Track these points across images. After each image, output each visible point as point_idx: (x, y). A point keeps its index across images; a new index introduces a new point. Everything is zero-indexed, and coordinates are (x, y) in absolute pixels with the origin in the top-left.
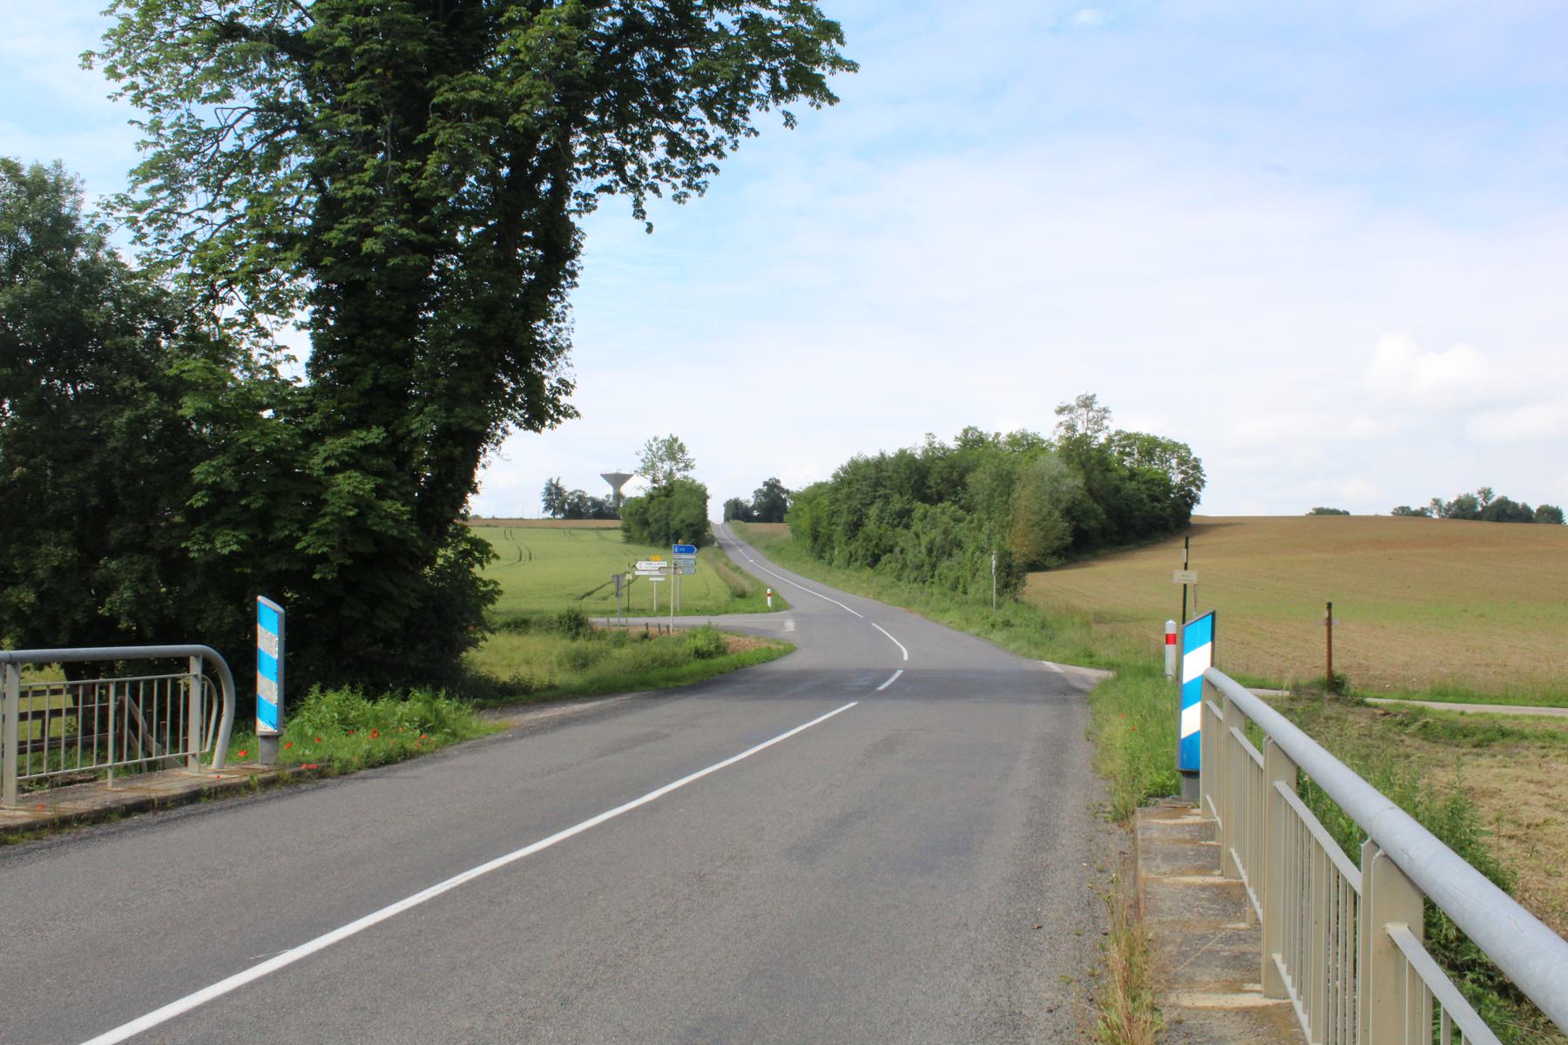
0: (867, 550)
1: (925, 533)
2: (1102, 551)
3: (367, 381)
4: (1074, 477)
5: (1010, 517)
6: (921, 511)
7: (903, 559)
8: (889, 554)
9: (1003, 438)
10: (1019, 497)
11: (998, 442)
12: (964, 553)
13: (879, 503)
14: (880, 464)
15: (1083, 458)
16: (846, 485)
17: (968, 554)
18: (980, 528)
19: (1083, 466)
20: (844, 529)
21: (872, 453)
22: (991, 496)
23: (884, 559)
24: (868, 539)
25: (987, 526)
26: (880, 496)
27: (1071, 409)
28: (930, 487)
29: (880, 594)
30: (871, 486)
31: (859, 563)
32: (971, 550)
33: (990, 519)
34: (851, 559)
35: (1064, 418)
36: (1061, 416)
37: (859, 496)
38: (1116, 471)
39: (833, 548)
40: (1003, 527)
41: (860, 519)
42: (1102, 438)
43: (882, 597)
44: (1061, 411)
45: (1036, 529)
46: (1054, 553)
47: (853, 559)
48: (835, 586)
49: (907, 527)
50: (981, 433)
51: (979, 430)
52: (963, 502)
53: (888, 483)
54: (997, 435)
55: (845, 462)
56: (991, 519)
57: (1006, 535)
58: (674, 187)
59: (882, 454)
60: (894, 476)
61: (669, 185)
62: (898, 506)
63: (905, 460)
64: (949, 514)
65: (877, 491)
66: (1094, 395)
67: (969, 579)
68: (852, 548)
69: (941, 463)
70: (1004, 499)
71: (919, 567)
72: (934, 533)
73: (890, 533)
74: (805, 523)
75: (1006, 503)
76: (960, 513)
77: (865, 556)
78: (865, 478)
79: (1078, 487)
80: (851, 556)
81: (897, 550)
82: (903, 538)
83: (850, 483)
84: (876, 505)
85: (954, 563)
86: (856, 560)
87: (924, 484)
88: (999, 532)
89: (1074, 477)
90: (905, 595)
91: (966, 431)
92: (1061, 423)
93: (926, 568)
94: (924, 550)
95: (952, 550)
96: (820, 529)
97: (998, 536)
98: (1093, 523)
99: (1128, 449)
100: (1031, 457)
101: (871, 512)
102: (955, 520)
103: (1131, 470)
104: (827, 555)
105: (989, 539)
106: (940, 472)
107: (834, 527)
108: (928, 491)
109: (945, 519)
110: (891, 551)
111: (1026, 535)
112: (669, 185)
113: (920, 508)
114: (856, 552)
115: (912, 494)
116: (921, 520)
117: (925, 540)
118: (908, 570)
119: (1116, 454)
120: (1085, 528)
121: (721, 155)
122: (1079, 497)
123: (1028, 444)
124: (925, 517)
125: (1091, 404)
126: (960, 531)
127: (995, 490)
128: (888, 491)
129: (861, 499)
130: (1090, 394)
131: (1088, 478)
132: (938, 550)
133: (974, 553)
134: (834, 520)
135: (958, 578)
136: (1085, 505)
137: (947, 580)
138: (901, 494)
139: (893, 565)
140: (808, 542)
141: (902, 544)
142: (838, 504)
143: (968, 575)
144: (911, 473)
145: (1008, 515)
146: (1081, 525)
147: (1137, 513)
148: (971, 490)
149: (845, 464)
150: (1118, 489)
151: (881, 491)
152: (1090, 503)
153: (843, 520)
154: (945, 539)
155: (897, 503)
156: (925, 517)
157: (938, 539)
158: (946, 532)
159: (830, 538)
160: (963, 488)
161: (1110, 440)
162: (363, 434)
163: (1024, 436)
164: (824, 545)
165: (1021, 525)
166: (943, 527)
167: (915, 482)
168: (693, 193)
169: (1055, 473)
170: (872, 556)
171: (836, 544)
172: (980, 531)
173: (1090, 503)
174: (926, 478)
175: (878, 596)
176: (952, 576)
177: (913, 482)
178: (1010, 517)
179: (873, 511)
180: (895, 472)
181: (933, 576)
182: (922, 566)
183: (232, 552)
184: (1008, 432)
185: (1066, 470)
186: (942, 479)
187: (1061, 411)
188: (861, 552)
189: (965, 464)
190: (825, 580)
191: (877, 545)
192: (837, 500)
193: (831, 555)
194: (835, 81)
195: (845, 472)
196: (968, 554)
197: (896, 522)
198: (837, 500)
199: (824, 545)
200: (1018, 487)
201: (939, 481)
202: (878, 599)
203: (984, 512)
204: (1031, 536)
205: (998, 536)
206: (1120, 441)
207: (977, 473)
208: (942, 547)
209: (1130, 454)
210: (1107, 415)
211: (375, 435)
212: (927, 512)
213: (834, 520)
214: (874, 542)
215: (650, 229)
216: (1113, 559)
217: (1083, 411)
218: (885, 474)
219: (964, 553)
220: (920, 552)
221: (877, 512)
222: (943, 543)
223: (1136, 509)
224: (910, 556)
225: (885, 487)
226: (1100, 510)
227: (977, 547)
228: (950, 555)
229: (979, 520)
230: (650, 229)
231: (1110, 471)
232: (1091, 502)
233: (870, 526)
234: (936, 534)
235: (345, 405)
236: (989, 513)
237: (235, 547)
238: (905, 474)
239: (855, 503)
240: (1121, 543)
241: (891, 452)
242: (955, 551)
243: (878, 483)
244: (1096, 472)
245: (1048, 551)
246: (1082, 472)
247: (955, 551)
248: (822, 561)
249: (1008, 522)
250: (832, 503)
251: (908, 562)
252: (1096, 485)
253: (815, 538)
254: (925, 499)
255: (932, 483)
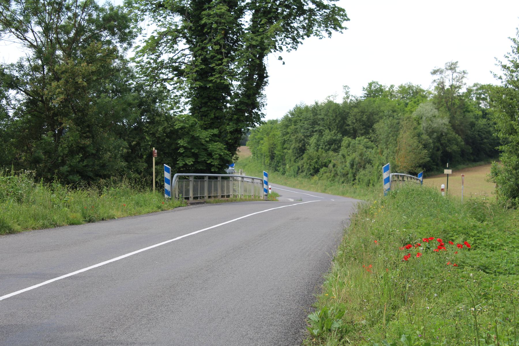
0: (310, 165)
1: (349, 155)
2: (461, 166)
3: (212, 116)
4: (442, 118)
5: (397, 148)
6: (347, 142)
7: (335, 170)
8: (324, 168)
9: (396, 89)
10: (402, 137)
11: (393, 91)
12: (373, 166)
13: (316, 136)
14: (316, 110)
15: (449, 104)
16: (293, 124)
17: (375, 167)
18: (382, 152)
19: (449, 110)
20: (293, 152)
21: (310, 103)
22: (388, 136)
23: (322, 170)
24: (310, 158)
25: (385, 152)
26: (316, 131)
27: (441, 72)
28: (348, 125)
29: (325, 189)
30: (310, 125)
31: (304, 174)
32: (377, 164)
33: (387, 148)
34: (299, 171)
35: (437, 77)
36: (435, 76)
37: (302, 131)
38: (472, 112)
39: (285, 164)
40: (394, 152)
41: (304, 145)
42: (463, 90)
43: (326, 191)
44: (435, 72)
45: (411, 153)
46: (420, 166)
47: (300, 171)
48: (294, 187)
49: (336, 150)
50: (381, 86)
51: (379, 84)
52: (372, 138)
53: (321, 122)
54: (392, 86)
55: (291, 108)
56: (388, 148)
57: (395, 157)
58: (287, 47)
59: (317, 103)
60: (326, 118)
61: (285, 47)
62: (329, 137)
63: (332, 108)
64: (363, 144)
65: (314, 128)
66: (457, 62)
67: (376, 180)
68: (300, 164)
69: (356, 110)
70: (395, 138)
71: (346, 175)
72: (354, 155)
73: (324, 155)
74: (265, 147)
75: (396, 140)
76: (370, 144)
77: (309, 169)
78: (306, 119)
79: (445, 124)
80: (299, 169)
81: (331, 165)
82: (335, 158)
83: (295, 122)
84: (314, 137)
85: (367, 172)
86: (302, 172)
87: (344, 123)
88: (392, 155)
89: (442, 118)
90: (341, 189)
91: (370, 85)
92: (435, 81)
93: (350, 175)
94: (348, 164)
95: (365, 165)
96: (276, 152)
97: (392, 157)
98: (455, 147)
99: (483, 96)
100: (415, 102)
101: (311, 142)
102: (367, 148)
103: (483, 111)
104: (281, 169)
105: (387, 159)
106: (355, 116)
107: (285, 151)
108: (347, 127)
109: (361, 147)
110: (326, 166)
111: (406, 157)
112: (285, 47)
113: (346, 140)
114: (303, 166)
115: (337, 130)
116: (347, 148)
117: (349, 159)
118: (338, 177)
119: (474, 99)
120: (450, 151)
121: (303, 39)
122: (445, 131)
123: (413, 93)
124: (349, 145)
125: (455, 68)
126: (370, 154)
127: (390, 133)
128: (321, 128)
129: (304, 132)
130: (454, 61)
131: (452, 118)
132: (357, 165)
133: (379, 166)
134: (285, 146)
135: (370, 180)
136: (449, 136)
137: (363, 182)
138: (330, 129)
139: (327, 174)
140: (267, 160)
141: (335, 162)
142: (288, 135)
143: (376, 178)
144: (336, 116)
145: (396, 147)
146: (447, 149)
147: (485, 141)
148: (378, 132)
149: (292, 109)
150: (473, 125)
151: (317, 128)
152: (453, 134)
153: (292, 147)
154: (361, 159)
155: (328, 136)
156: (349, 145)
157: (357, 159)
158: (361, 155)
159: (283, 158)
160: (373, 131)
161: (469, 91)
162: (212, 131)
163: (410, 87)
164: (278, 162)
165: (402, 152)
166: (360, 152)
167: (339, 121)
168: (294, 50)
169: (429, 115)
170: (313, 169)
171: (287, 161)
172: (382, 154)
173: (453, 134)
174: (346, 119)
175: (324, 191)
176: (366, 179)
177: (337, 122)
178: (397, 148)
179: (313, 140)
180: (326, 115)
181: (355, 179)
182: (347, 174)
183: (191, 164)
184: (400, 84)
185: (436, 113)
186: (356, 119)
187: (435, 72)
188: (306, 166)
189: (370, 110)
190: (286, 184)
191: (316, 162)
192: (288, 133)
193: (284, 169)
194: (344, 24)
195: (292, 114)
196: (375, 167)
197: (327, 147)
198: (288, 133)
199: (278, 162)
200: (401, 132)
201: (354, 121)
202: (324, 192)
203: (385, 144)
204: (408, 158)
205: (392, 157)
206: (477, 90)
207: (380, 123)
208: (359, 163)
209: (484, 99)
210: (465, 75)
211: (216, 131)
212: (350, 143)
213: (285, 146)
214: (315, 161)
215: (284, 63)
216: (468, 171)
217: (449, 72)
218: (319, 117)
219: (373, 166)
220: (345, 166)
221: (315, 141)
222: (360, 161)
223: (485, 138)
224: (339, 169)
225: (319, 125)
226: (460, 139)
227: (380, 163)
228: (364, 168)
229: (381, 148)
230: (284, 63)
231: (469, 112)
232: (454, 133)
233: (311, 150)
234: (355, 156)
235: (206, 122)
236: (387, 145)
237: (192, 163)
238: (332, 116)
239: (300, 135)
240: (475, 161)
241: (322, 100)
242: (367, 166)
243: (314, 123)
244: (458, 113)
245: (417, 165)
246: (448, 114)
247: (367, 166)
248: (277, 172)
249: (396, 151)
250: (284, 135)
251: (338, 172)
252: (457, 122)
253: (272, 157)
254: (345, 133)
255: (350, 123)
